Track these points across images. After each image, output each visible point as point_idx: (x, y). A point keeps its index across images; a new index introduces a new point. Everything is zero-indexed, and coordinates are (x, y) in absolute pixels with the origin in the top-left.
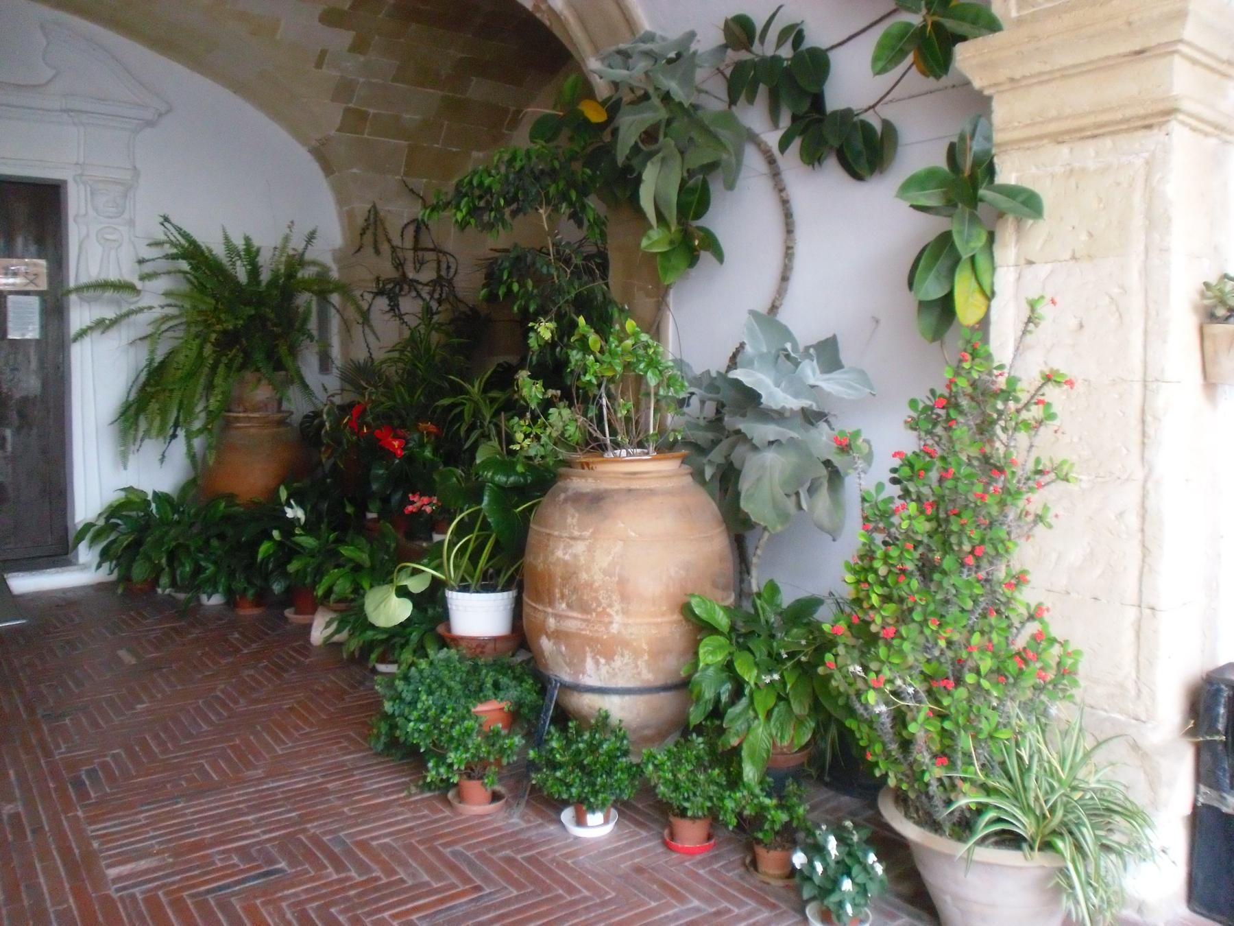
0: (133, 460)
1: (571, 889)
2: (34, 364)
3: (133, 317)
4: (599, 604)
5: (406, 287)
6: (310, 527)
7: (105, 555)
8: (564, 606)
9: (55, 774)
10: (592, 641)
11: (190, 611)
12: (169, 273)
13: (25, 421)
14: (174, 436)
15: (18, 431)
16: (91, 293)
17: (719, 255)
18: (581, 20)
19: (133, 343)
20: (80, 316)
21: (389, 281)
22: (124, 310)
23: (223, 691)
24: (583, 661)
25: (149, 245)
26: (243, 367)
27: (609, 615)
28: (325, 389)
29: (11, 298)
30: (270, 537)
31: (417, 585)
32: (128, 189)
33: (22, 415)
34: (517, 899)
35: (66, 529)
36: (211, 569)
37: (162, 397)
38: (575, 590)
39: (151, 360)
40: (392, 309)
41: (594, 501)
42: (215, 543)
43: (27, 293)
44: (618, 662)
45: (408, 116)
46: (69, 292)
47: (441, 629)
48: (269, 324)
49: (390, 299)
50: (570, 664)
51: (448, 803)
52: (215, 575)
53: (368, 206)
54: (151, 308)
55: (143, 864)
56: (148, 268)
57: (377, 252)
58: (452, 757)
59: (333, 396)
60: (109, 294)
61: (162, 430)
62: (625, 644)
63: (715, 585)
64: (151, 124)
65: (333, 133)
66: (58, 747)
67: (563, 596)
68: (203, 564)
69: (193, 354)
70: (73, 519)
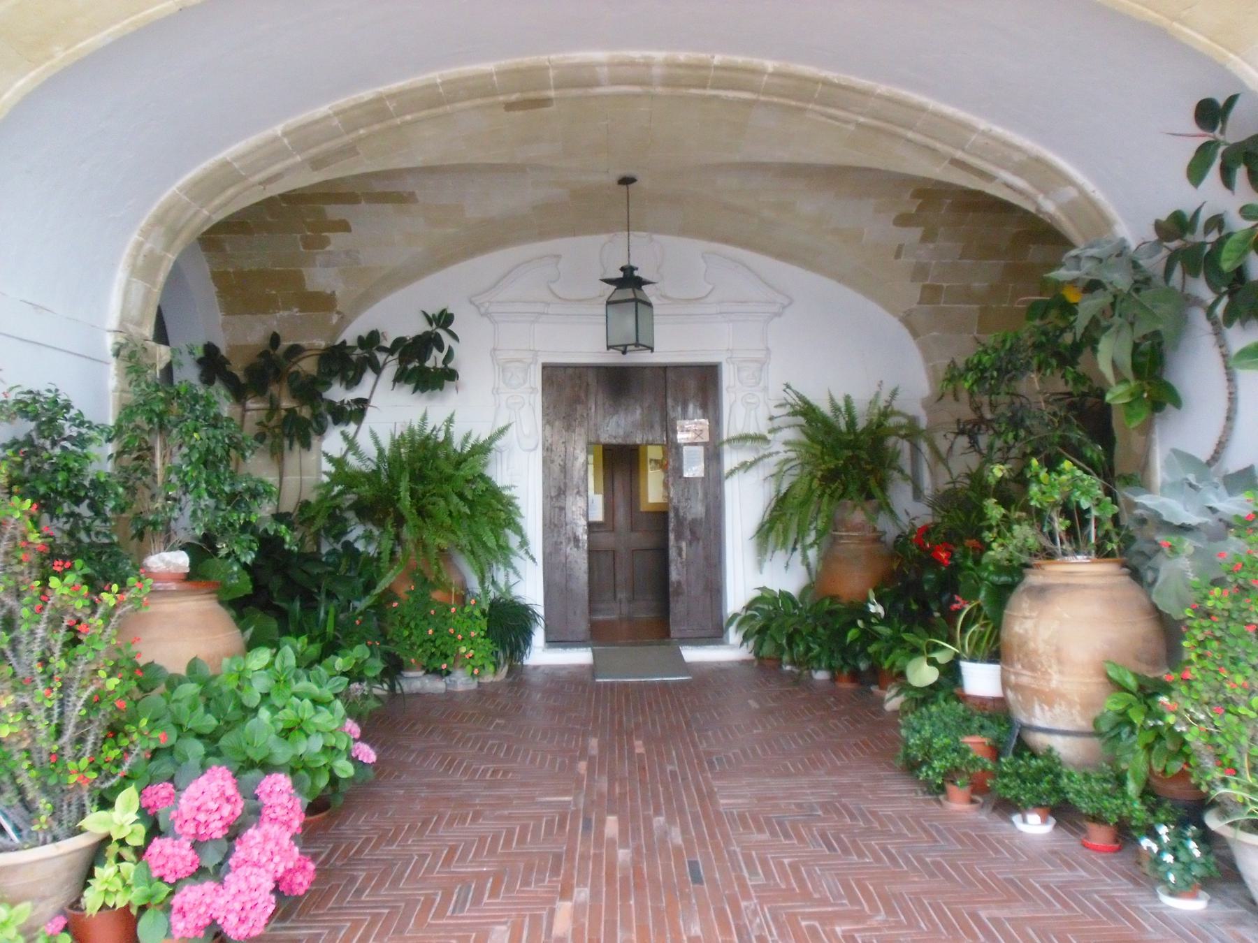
0: (767, 565)
1: (997, 851)
2: (700, 495)
3: (766, 460)
4: (1042, 665)
5: (983, 427)
6: (886, 621)
7: (746, 638)
8: (1020, 666)
9: (698, 757)
10: (1037, 692)
11: (809, 684)
12: (789, 427)
13: (695, 538)
14: (794, 549)
15: (690, 544)
16: (736, 444)
17: (1177, 403)
18: (1071, 219)
19: (765, 479)
20: (731, 459)
21: (969, 422)
22: (761, 454)
23: (813, 730)
24: (1033, 707)
25: (776, 407)
26: (842, 496)
27: (1049, 674)
28: (907, 514)
29: (685, 448)
30: (857, 626)
31: (942, 657)
32: (762, 364)
33: (693, 532)
34: (960, 851)
35: (721, 617)
36: (816, 649)
37: (783, 519)
38: (1026, 655)
39: (778, 491)
40: (972, 446)
41: (1041, 592)
42: (820, 630)
43: (696, 444)
44: (1057, 710)
45: (976, 284)
46: (722, 443)
47: (956, 691)
48: (863, 463)
49: (970, 437)
50: (1025, 710)
51: (939, 802)
52: (819, 654)
53: (947, 361)
54: (777, 453)
55: (740, 801)
56: (776, 423)
57: (956, 399)
58: (936, 764)
59: (914, 519)
60: (749, 443)
61: (784, 544)
62: (1062, 696)
63: (1138, 659)
64: (778, 315)
65: (915, 306)
66: (701, 743)
67: (1019, 660)
68: (812, 645)
69: (806, 487)
70: (726, 610)
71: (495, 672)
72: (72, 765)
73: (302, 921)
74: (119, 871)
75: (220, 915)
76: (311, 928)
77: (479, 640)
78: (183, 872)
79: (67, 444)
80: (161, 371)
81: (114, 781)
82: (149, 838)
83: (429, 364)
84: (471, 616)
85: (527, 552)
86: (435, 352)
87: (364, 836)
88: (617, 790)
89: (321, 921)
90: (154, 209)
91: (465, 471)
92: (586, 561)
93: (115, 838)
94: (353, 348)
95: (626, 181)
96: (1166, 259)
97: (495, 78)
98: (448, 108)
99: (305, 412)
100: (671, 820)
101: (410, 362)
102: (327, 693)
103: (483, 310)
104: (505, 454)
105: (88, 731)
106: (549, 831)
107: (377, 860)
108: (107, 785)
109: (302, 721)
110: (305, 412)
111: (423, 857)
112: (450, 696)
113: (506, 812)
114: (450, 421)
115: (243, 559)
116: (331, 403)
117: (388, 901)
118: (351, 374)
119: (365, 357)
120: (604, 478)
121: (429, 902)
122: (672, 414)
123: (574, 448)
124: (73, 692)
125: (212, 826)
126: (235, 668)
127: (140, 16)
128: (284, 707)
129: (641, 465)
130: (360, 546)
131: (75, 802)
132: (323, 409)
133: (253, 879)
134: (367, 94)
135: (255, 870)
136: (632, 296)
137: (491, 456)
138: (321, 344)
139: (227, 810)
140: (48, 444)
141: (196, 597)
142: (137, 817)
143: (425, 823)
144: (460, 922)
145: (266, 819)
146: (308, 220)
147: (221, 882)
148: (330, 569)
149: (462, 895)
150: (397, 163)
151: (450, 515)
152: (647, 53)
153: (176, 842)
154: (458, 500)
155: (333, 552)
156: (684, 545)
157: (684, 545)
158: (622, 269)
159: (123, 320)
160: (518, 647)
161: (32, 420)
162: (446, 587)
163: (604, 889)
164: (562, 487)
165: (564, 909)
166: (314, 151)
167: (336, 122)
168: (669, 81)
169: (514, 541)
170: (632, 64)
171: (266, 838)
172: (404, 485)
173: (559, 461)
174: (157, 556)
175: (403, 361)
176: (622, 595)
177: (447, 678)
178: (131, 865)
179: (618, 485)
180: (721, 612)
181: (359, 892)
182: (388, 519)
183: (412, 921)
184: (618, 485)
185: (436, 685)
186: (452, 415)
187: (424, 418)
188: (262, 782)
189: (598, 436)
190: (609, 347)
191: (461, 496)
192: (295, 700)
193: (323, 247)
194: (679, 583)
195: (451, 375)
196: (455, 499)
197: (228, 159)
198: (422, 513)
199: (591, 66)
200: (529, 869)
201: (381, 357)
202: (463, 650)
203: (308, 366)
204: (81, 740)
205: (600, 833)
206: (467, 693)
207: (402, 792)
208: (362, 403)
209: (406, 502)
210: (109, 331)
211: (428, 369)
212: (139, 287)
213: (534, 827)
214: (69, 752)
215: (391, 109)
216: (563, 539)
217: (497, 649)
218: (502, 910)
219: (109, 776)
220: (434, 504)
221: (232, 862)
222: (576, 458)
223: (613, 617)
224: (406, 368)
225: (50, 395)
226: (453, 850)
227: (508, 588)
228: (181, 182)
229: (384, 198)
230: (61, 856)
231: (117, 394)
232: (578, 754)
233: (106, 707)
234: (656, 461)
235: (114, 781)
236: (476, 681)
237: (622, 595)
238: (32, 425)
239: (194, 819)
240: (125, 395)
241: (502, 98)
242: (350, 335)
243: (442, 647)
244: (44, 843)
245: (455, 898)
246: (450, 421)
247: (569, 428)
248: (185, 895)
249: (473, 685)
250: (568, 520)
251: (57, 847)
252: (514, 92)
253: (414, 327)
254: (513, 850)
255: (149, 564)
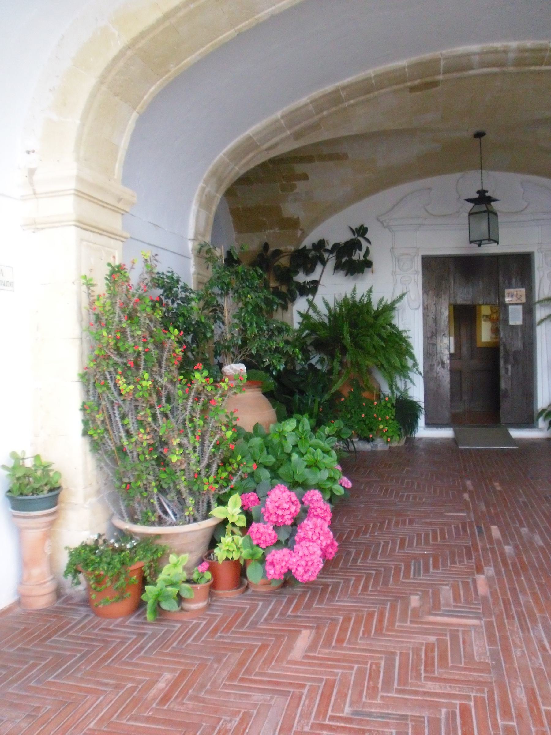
15: (513, 366)
16: (546, 303)
20: (540, 313)
33: (515, 358)
35: (533, 412)
43: (517, 304)
70: (537, 406)
71: (399, 442)
72: (205, 480)
73: (326, 574)
74: (233, 540)
75: (293, 568)
76: (333, 578)
77: (391, 421)
78: (270, 542)
79: (179, 302)
80: (225, 260)
81: (227, 490)
82: (249, 522)
83: (355, 258)
84: (385, 407)
85: (417, 370)
86: (358, 251)
87: (349, 529)
88: (492, 511)
89: (336, 575)
90: (210, 167)
91: (381, 321)
92: (449, 376)
93: (230, 521)
94: (310, 250)
95: (479, 135)
96: (289, 324)
97: (406, 70)
98: (376, 93)
99: (284, 289)
100: (531, 530)
101: (343, 257)
102: (328, 447)
103: (385, 224)
104: (400, 312)
105: (214, 461)
106: (458, 534)
107: (360, 543)
108: (222, 492)
109: (316, 461)
110: (284, 289)
111: (386, 543)
112: (374, 453)
113: (428, 520)
114: (370, 291)
115: (278, 368)
116: (298, 283)
117: (374, 567)
118: (309, 266)
119: (317, 256)
120: (455, 327)
121: (398, 570)
122: (501, 285)
123: (441, 308)
124: (207, 438)
125: (286, 517)
126: (277, 430)
127: (216, 41)
128: (306, 453)
129: (477, 319)
130: (319, 367)
131: (206, 500)
132: (293, 287)
133: (311, 548)
134: (329, 88)
135: (311, 544)
136: (486, 209)
137: (394, 313)
138: (292, 248)
139: (293, 509)
140: (170, 302)
141: (251, 390)
142: (240, 511)
143: (382, 523)
144: (419, 582)
145: (311, 515)
146: (284, 174)
147: (291, 549)
148: (303, 379)
149: (417, 566)
150: (343, 133)
151: (374, 347)
152: (505, 44)
153: (265, 525)
154: (378, 338)
155: (303, 370)
156: (509, 367)
157: (509, 367)
158: (478, 192)
159: (196, 233)
160: (413, 425)
161: (161, 288)
162: (370, 389)
163: (503, 569)
164: (434, 331)
165: (481, 579)
166: (297, 128)
167: (311, 107)
168: (519, 62)
169: (410, 363)
170: (496, 51)
171: (316, 526)
172: (346, 328)
173: (432, 316)
174: (229, 366)
175: (338, 258)
176: (465, 397)
177: (371, 443)
178: (239, 537)
179: (463, 332)
180: (533, 409)
181: (355, 560)
182: (337, 350)
183: (391, 580)
184: (463, 332)
185: (366, 447)
186: (371, 288)
187: (354, 290)
188: (306, 494)
189: (456, 301)
190: (471, 242)
191: (379, 336)
192: (312, 449)
193: (292, 190)
194: (506, 390)
195: (367, 264)
196: (376, 338)
197: (251, 134)
198: (358, 346)
199: (469, 55)
200: (453, 554)
201: (326, 255)
202: (381, 427)
203: (284, 261)
204: (209, 466)
205: (490, 537)
206: (384, 452)
207: (363, 506)
208: (316, 283)
209: (347, 340)
210: (190, 240)
211: (354, 261)
212: (203, 213)
213: (448, 529)
214: (203, 473)
215: (343, 97)
216: (435, 363)
217: (401, 427)
218: (442, 577)
219: (222, 487)
220: (364, 341)
221: (296, 538)
222: (442, 314)
223: (461, 411)
224: (341, 261)
225: (169, 274)
226: (403, 541)
227: (406, 390)
228: (225, 150)
229: (331, 157)
230: (199, 530)
231: (195, 276)
232: (461, 489)
233: (223, 447)
234: (487, 316)
235: (227, 490)
236: (388, 445)
237: (465, 397)
238: (161, 291)
239: (276, 513)
240: (199, 277)
241: (409, 84)
242: (308, 242)
243: (370, 424)
244: (189, 522)
245: (412, 568)
246: (370, 291)
247: (438, 295)
248: (274, 555)
249: (387, 448)
250: (438, 351)
251: (199, 525)
252: (416, 79)
253: (344, 237)
254: (439, 543)
255: (225, 371)
